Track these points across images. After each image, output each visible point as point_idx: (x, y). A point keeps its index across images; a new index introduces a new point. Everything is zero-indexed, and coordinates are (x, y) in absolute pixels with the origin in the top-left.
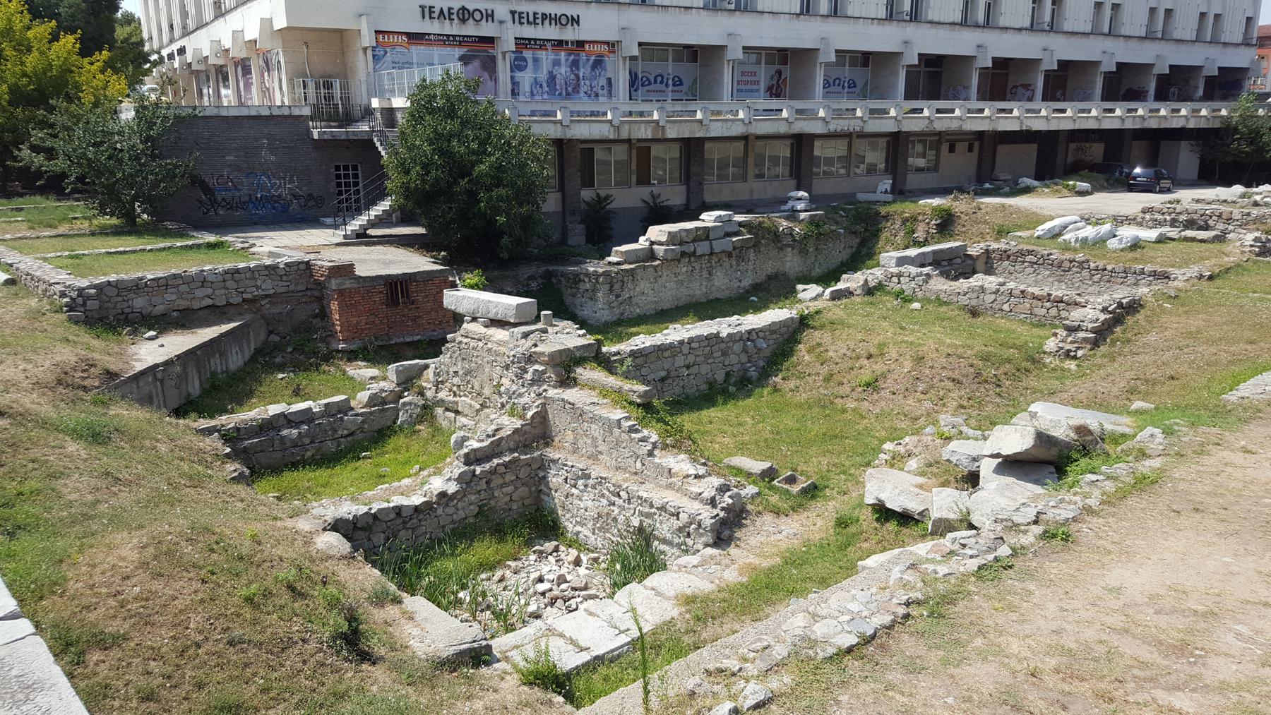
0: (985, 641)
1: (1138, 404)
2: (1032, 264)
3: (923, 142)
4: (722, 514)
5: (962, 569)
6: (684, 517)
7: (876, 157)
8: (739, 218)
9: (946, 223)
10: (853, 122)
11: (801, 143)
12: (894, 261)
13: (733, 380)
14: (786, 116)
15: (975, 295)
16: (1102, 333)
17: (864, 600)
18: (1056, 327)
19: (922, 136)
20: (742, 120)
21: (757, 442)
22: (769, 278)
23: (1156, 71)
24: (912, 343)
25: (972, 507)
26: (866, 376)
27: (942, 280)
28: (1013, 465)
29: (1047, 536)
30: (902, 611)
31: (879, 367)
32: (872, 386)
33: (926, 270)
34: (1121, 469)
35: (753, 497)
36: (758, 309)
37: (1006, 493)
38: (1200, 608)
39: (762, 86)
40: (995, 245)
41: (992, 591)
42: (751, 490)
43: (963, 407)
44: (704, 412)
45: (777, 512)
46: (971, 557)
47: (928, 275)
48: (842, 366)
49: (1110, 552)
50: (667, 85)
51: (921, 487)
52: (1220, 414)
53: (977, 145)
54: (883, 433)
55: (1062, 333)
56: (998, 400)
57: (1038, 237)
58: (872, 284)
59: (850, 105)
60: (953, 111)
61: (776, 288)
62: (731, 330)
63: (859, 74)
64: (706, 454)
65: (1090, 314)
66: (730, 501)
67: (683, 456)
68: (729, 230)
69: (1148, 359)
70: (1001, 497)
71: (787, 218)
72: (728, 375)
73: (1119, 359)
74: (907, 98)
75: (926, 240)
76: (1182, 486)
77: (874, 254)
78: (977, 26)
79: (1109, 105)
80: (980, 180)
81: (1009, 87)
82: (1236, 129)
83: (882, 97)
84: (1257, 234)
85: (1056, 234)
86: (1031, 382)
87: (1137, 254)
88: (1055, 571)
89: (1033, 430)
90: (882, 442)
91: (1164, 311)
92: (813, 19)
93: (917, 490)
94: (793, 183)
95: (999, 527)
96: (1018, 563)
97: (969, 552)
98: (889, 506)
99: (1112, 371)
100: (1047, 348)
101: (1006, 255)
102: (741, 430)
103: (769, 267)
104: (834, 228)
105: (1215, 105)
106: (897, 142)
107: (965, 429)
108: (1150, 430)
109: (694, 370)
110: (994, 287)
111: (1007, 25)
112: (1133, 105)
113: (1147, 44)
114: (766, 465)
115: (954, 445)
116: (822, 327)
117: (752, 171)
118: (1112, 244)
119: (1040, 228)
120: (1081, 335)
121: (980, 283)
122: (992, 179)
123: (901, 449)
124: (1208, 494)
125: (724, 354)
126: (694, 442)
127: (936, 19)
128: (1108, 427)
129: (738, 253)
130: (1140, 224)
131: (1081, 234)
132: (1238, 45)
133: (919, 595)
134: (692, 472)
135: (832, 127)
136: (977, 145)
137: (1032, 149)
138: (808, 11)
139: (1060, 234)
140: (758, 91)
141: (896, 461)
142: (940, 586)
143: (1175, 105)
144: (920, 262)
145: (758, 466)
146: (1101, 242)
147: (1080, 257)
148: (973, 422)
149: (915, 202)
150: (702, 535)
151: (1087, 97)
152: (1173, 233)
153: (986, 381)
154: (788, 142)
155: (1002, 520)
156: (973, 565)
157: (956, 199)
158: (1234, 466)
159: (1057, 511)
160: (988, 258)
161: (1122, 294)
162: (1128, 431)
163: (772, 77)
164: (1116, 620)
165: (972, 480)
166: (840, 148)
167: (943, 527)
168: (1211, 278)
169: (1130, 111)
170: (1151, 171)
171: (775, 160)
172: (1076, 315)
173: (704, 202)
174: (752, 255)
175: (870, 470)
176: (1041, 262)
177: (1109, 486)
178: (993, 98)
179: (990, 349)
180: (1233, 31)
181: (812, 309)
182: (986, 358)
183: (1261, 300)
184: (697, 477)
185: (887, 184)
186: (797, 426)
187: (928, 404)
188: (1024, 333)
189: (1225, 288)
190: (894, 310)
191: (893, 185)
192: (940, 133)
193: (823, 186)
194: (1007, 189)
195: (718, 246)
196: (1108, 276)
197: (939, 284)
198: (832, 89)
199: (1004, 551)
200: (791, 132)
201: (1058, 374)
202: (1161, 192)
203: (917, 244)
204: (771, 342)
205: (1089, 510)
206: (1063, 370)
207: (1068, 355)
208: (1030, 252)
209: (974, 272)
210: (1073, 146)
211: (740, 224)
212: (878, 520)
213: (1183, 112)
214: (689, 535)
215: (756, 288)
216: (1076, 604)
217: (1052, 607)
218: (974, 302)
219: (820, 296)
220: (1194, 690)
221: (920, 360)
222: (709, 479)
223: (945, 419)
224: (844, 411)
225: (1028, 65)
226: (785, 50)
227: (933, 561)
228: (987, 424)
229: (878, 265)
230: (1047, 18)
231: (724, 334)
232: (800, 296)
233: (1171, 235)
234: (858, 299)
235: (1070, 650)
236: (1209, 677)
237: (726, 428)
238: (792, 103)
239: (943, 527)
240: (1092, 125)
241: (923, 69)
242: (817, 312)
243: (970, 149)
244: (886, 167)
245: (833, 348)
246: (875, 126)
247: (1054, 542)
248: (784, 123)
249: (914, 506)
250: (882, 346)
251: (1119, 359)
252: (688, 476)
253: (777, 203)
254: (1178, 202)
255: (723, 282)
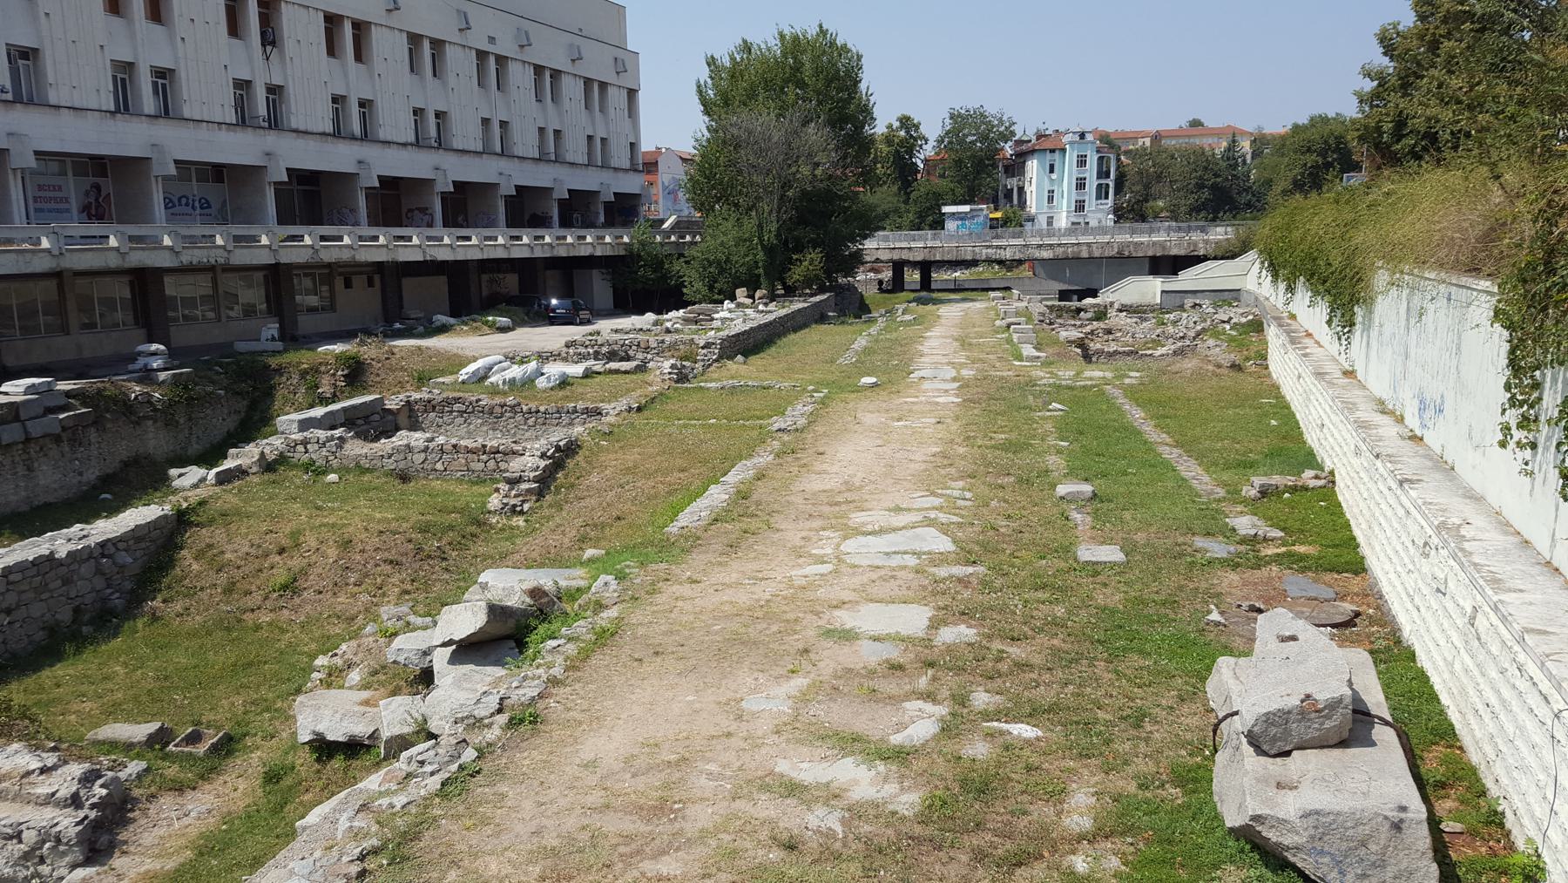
0: (460, 872)
1: (590, 553)
2: (461, 413)
3: (313, 276)
4: (93, 814)
5: (423, 792)
6: (30, 837)
7: (253, 295)
8: (64, 386)
9: (356, 374)
10: (213, 253)
11: (144, 281)
12: (295, 425)
13: (87, 617)
14: (115, 243)
15: (402, 456)
16: (545, 481)
17: (306, 871)
18: (498, 481)
19: (308, 269)
20: (47, 251)
21: (136, 698)
22: (126, 464)
23: (556, 196)
24: (333, 525)
25: (428, 712)
26: (281, 576)
27: (359, 442)
28: (469, 650)
29: (513, 723)
30: (355, 869)
31: (296, 563)
32: (290, 587)
33: (338, 433)
34: (580, 627)
35: (139, 776)
36: (113, 510)
37: (465, 685)
38: (673, 757)
39: (74, 206)
40: (416, 396)
41: (461, 808)
42: (134, 767)
43: (407, 592)
44: (46, 673)
45: (179, 788)
46: (432, 774)
47: (340, 438)
48: (246, 570)
49: (580, 723)
50: (194, 208)
51: (366, 703)
52: (668, 549)
53: (377, 278)
54: (313, 646)
55: (504, 487)
56: (446, 576)
57: (463, 382)
58: (271, 457)
59: (207, 231)
60: (340, 238)
61: (143, 478)
62: (72, 547)
63: (212, 191)
64: (56, 733)
65: (529, 463)
66: (104, 792)
67: (15, 746)
68: (52, 404)
69: (593, 502)
70: (461, 690)
71: (140, 381)
72: (77, 611)
73: (566, 507)
74: (280, 222)
75: (334, 395)
76: (641, 631)
77: (272, 418)
78: (354, 138)
79: (515, 232)
80: (389, 321)
81: (404, 211)
82: (639, 256)
83: (249, 221)
84: (672, 361)
85: (481, 377)
86: (480, 548)
87: (567, 392)
88: (527, 762)
89: (483, 604)
90: (314, 657)
91: (601, 449)
92: (135, 119)
93: (363, 709)
94: (142, 332)
95: (460, 728)
96: (486, 766)
97: (428, 768)
98: (330, 737)
99: (561, 522)
100: (491, 507)
101: (430, 406)
102: (110, 685)
103: (123, 449)
104: (210, 389)
105: (618, 231)
106: (277, 277)
107: (412, 618)
108: (603, 578)
109: (20, 614)
110: (421, 444)
111: (389, 138)
112: (539, 232)
113: (543, 167)
114: (153, 727)
115: (398, 642)
116: (211, 522)
117: (74, 319)
118: (541, 383)
119: (464, 371)
120: (525, 486)
121: (405, 442)
122: (402, 319)
123: (338, 661)
124: (665, 633)
125: (67, 581)
126: (33, 721)
127: (302, 128)
128: (563, 583)
129: (72, 434)
130: (565, 360)
131: (509, 375)
132: (626, 170)
133: (375, 842)
134: (35, 764)
135: (186, 258)
136: (377, 278)
137: (441, 282)
138: (127, 108)
139: (485, 377)
140: (68, 211)
141: (333, 678)
142: (399, 822)
143: (581, 232)
144: (329, 422)
145: (140, 731)
146: (529, 381)
147: (510, 400)
148: (420, 608)
149: (313, 350)
150: (64, 854)
151: (491, 224)
152: (598, 366)
153: (429, 557)
154: (126, 279)
155: (462, 719)
156: (434, 783)
157: (362, 343)
158: (684, 599)
159: (521, 692)
160: (411, 410)
161: (558, 436)
162: (582, 583)
163: (87, 194)
164: (595, 798)
165: (426, 678)
166: (202, 286)
167: (400, 744)
168: (639, 409)
169: (537, 238)
170: (568, 302)
171: (109, 303)
172: (515, 465)
173: (4, 367)
174: (93, 435)
175: (299, 699)
176: (471, 410)
177: (571, 649)
178: (387, 223)
179: (429, 517)
180: (621, 158)
181: (193, 500)
182: (424, 529)
183: (685, 426)
184: (44, 770)
185: (272, 329)
186: (194, 661)
187: (365, 598)
188: (465, 494)
189: (653, 418)
190: (305, 486)
191: (282, 329)
192: (329, 265)
193: (185, 336)
194: (421, 329)
195: (36, 428)
196: (543, 419)
197: (357, 449)
198: (177, 210)
199: (469, 754)
200: (127, 265)
201: (506, 534)
202: (581, 324)
203: (324, 401)
204: (138, 554)
205: (554, 682)
206: (512, 528)
207: (514, 511)
208: (457, 400)
209: (398, 429)
210: (485, 277)
211: (68, 394)
212: (318, 760)
213: (589, 239)
214: (42, 860)
215: (106, 482)
216: (553, 793)
217: (528, 805)
218: (402, 465)
219: (203, 480)
220: (678, 849)
221: (346, 544)
222: (66, 769)
223: (387, 611)
224: (258, 628)
225: (420, 185)
226: (101, 157)
227: (388, 793)
228: (431, 613)
229: (275, 432)
230: (433, 132)
231: (62, 553)
232: (176, 483)
233: (596, 368)
234: (256, 479)
235: (553, 849)
236: (691, 829)
237: (84, 688)
238: (121, 227)
239: (400, 744)
240: (500, 254)
241: (295, 187)
242: (202, 503)
243: (371, 283)
244: (269, 306)
245: (229, 547)
246: (242, 257)
247: (522, 729)
248: (115, 253)
249: (361, 729)
250: (295, 535)
251: (566, 507)
252: (29, 773)
253: (122, 361)
254: (599, 333)
255: (50, 478)
